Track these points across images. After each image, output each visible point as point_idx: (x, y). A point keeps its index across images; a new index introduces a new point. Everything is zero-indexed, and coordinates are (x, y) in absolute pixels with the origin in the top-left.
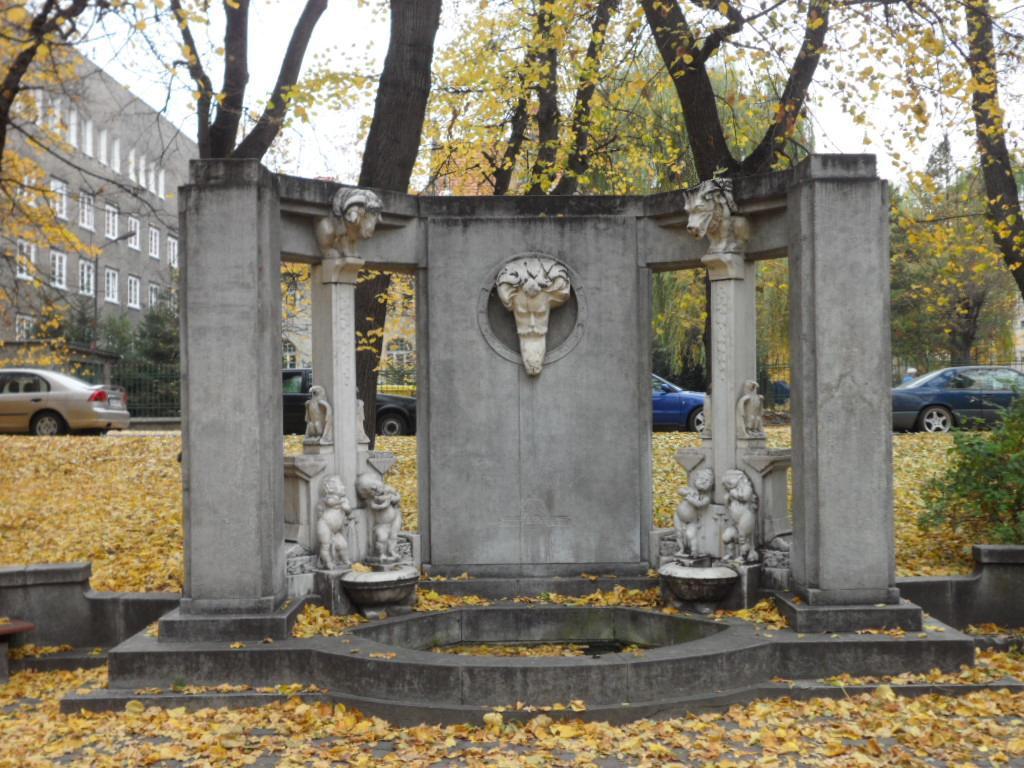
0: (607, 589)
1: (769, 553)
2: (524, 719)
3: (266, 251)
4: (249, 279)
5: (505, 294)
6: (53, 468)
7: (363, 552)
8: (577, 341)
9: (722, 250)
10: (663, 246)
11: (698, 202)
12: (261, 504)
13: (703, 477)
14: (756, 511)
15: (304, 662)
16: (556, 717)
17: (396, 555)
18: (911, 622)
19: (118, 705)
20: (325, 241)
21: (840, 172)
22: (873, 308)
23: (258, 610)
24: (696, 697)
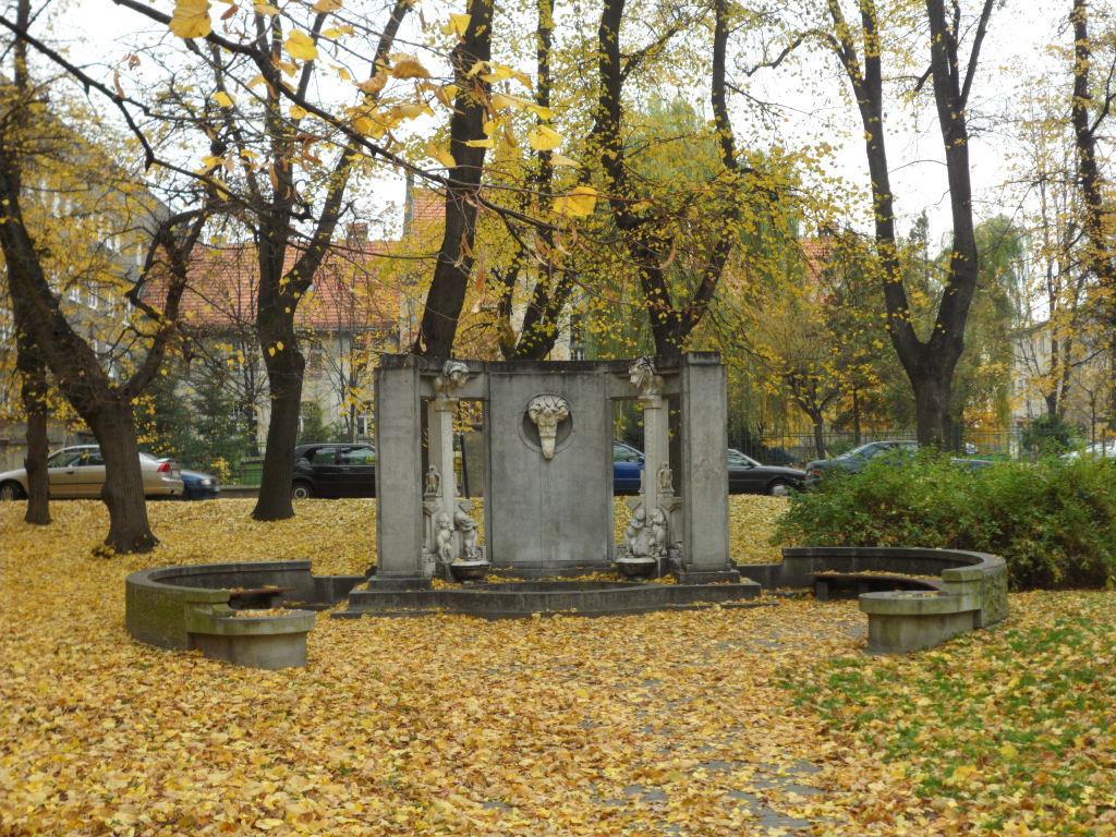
2: (550, 615)
5: (533, 415)
8: (572, 440)
9: (649, 393)
10: (618, 388)
13: (640, 513)
15: (442, 598)
16: (564, 615)
19: (358, 616)
21: (702, 360)
22: (718, 428)
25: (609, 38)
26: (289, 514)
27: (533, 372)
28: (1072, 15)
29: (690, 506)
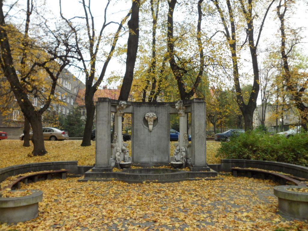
0: (162, 166)
1: (188, 160)
2: (149, 182)
3: (109, 111)
4: (107, 116)
5: (146, 118)
6: (56, 147)
7: (122, 159)
9: (181, 112)
10: (172, 110)
11: (177, 104)
12: (108, 151)
13: (178, 148)
14: (186, 153)
15: (115, 175)
16: (154, 182)
17: (128, 160)
18: (208, 170)
19: (86, 181)
20: (117, 109)
21: (198, 101)
23: (107, 167)
24: (175, 180)
25: (171, 11)
26: (90, 145)
27: (147, 105)
28: (280, 28)
29: (194, 146)
